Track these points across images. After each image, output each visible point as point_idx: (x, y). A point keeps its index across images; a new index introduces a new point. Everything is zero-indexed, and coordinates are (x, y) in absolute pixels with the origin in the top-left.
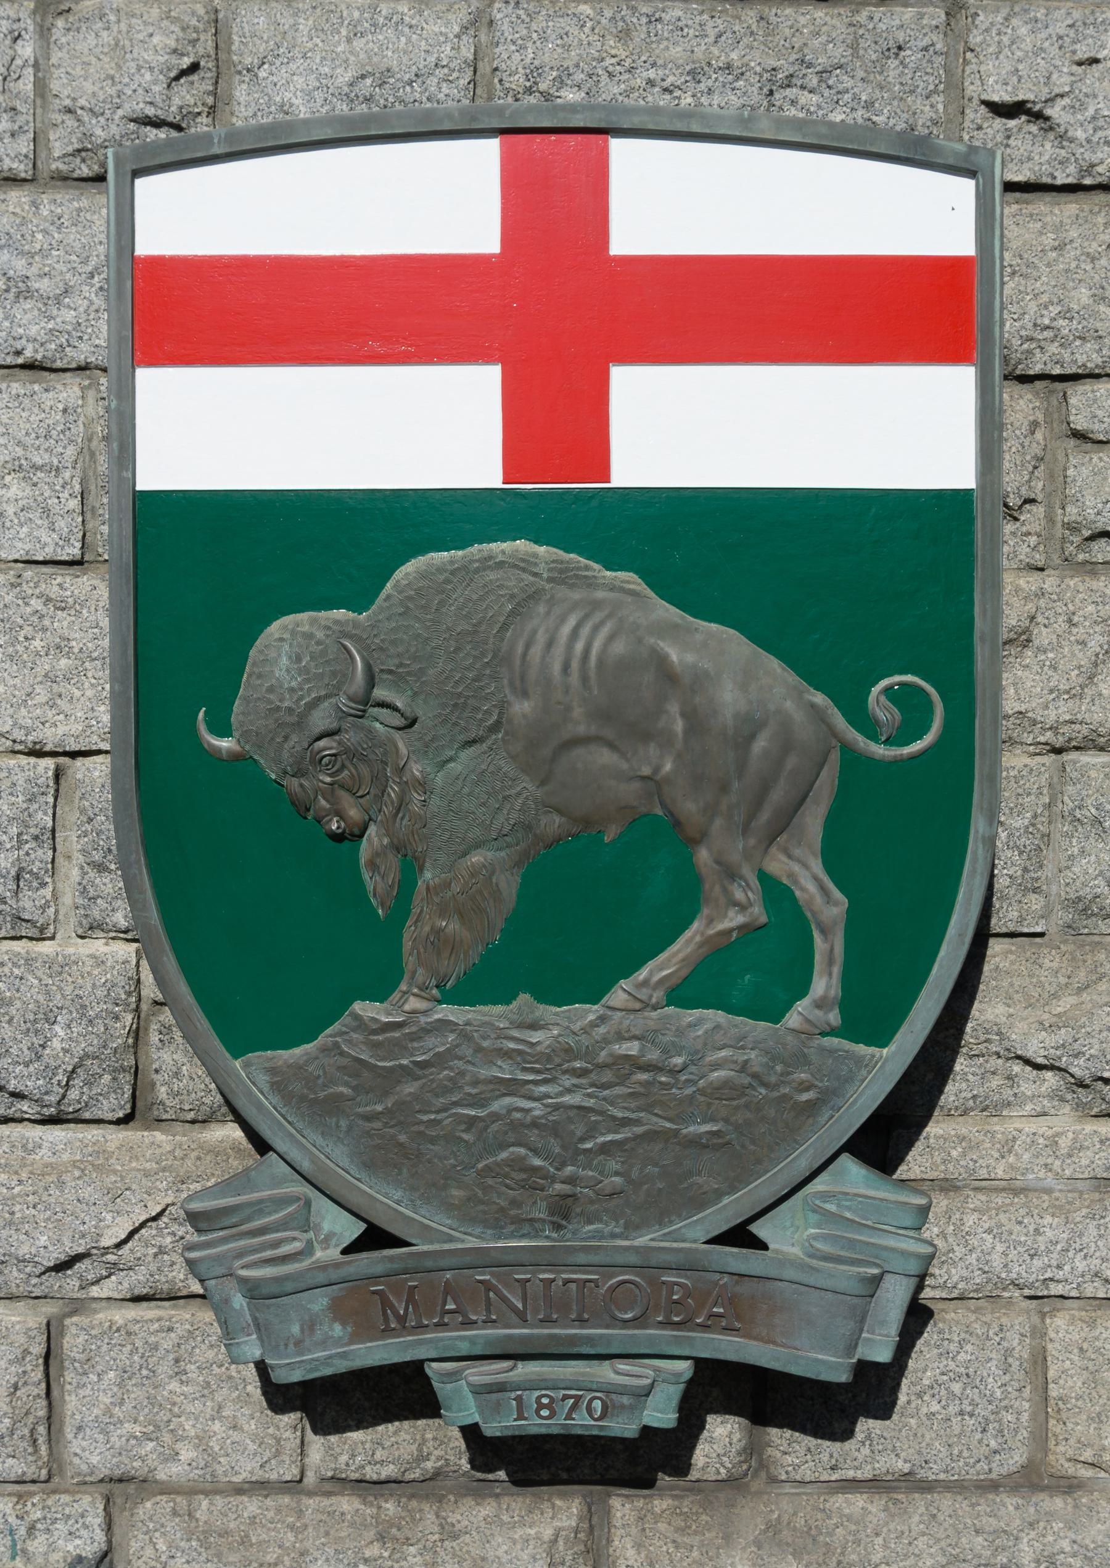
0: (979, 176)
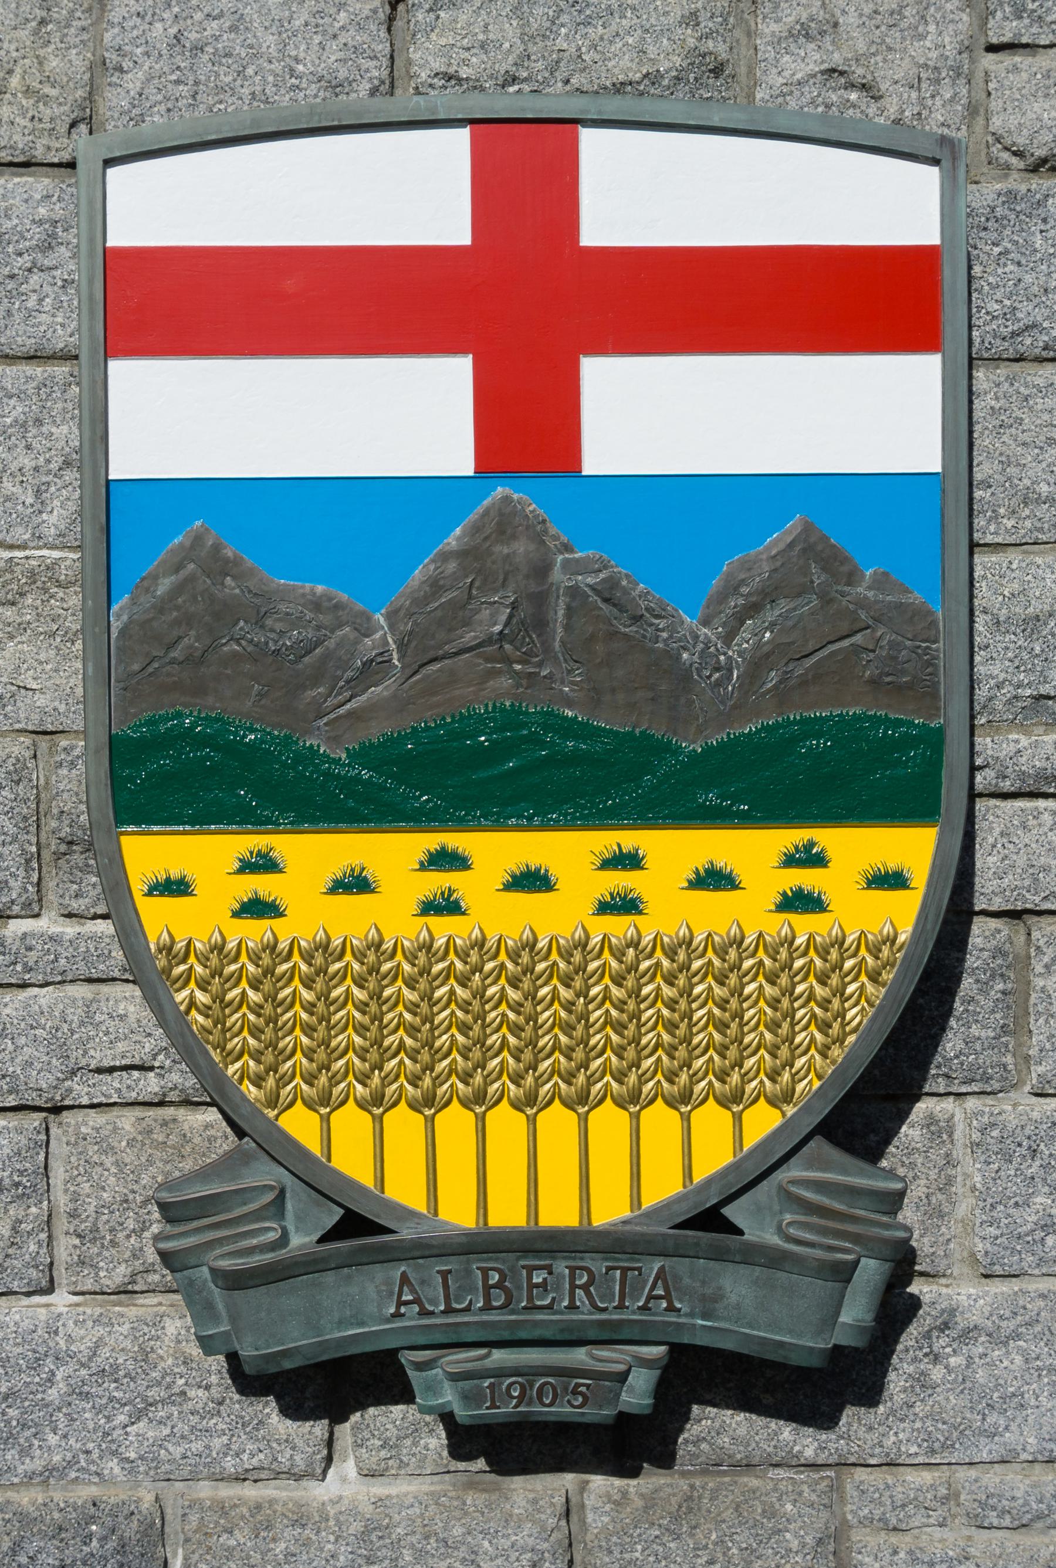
0: (943, 162)
